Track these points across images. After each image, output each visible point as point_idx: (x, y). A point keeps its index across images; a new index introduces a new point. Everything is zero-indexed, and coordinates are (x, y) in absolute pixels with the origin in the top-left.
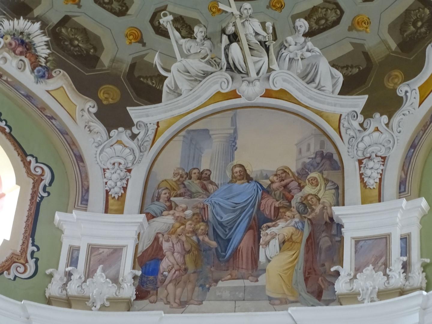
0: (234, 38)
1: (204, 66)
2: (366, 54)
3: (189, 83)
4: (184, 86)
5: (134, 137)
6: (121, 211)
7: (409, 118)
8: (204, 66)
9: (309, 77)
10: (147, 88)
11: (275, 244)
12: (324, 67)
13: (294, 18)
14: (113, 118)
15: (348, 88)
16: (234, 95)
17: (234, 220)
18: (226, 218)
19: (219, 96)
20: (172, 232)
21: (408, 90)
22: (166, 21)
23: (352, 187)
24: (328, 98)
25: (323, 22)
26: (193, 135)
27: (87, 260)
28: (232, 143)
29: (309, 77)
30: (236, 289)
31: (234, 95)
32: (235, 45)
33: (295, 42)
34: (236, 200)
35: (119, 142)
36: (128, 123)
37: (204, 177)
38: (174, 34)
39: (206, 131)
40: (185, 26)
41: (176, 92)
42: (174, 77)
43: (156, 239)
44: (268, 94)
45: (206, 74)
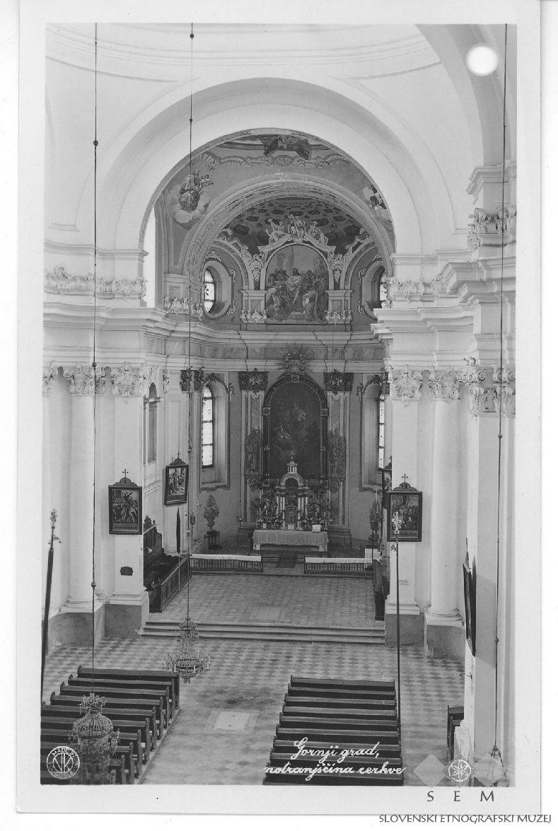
0: (293, 225)
1: (283, 233)
2: (336, 234)
3: (277, 238)
4: (276, 239)
5: (260, 257)
6: (259, 289)
7: (350, 255)
8: (283, 233)
9: (317, 237)
10: (265, 241)
11: (307, 300)
12: (322, 235)
13: (313, 221)
14: (254, 251)
15: (330, 244)
16: (292, 241)
17: (295, 291)
18: (292, 289)
19: (287, 242)
20: (276, 294)
21: (350, 247)
22: (270, 220)
23: (331, 285)
24: (322, 244)
25: (376, 651)
26: (280, 256)
27: (506, 717)
28: (292, 259)
29: (317, 237)
30: (297, 315)
31: (292, 241)
32: (293, 228)
33: (312, 227)
34: (295, 283)
35: (256, 260)
36: (258, 253)
37: (284, 272)
38: (272, 224)
39: (283, 255)
40: (276, 222)
41: (274, 241)
42: (272, 236)
43: (271, 296)
44: (304, 242)
45: (283, 235)
